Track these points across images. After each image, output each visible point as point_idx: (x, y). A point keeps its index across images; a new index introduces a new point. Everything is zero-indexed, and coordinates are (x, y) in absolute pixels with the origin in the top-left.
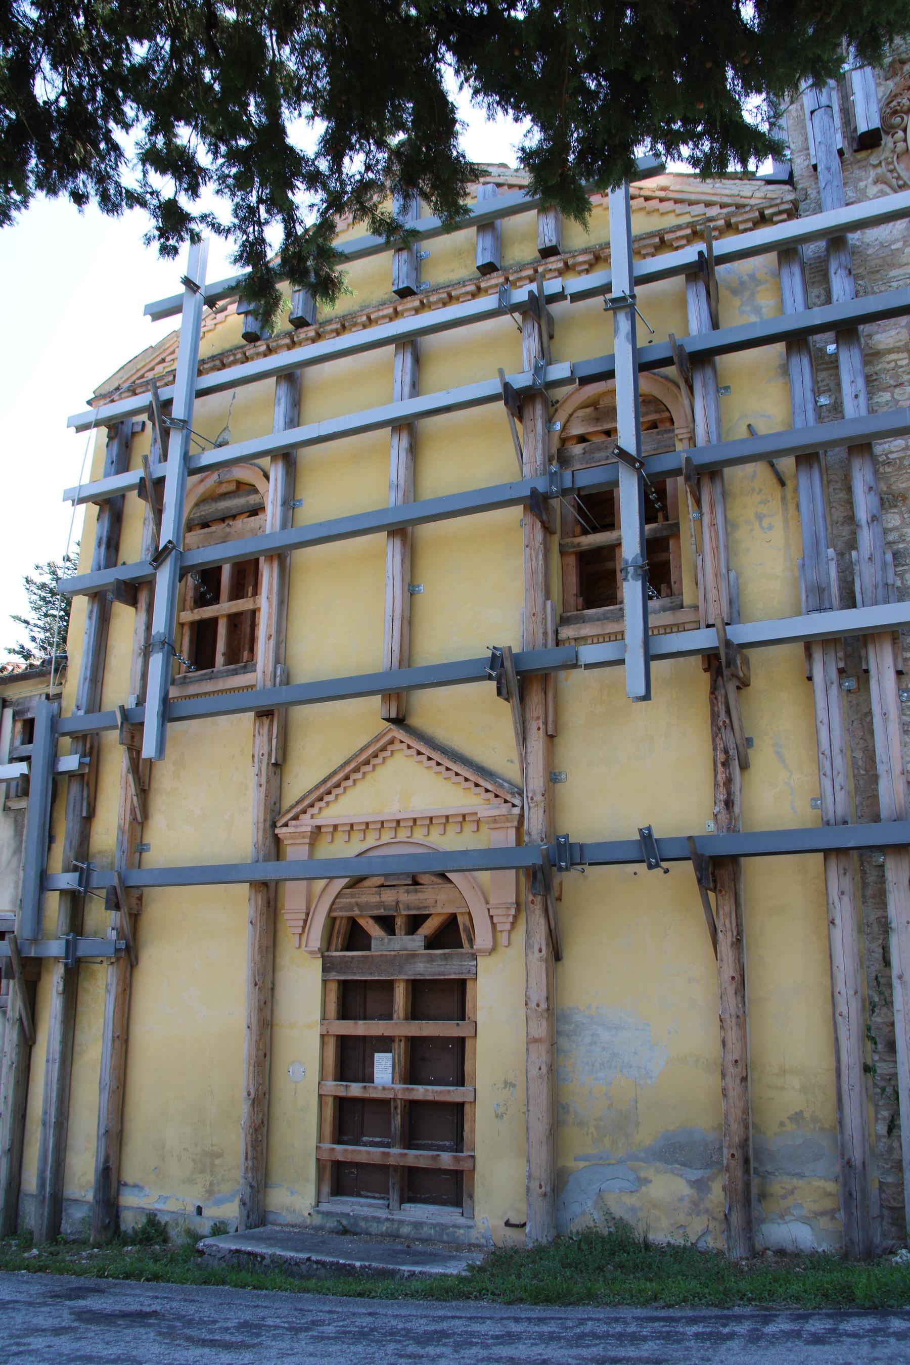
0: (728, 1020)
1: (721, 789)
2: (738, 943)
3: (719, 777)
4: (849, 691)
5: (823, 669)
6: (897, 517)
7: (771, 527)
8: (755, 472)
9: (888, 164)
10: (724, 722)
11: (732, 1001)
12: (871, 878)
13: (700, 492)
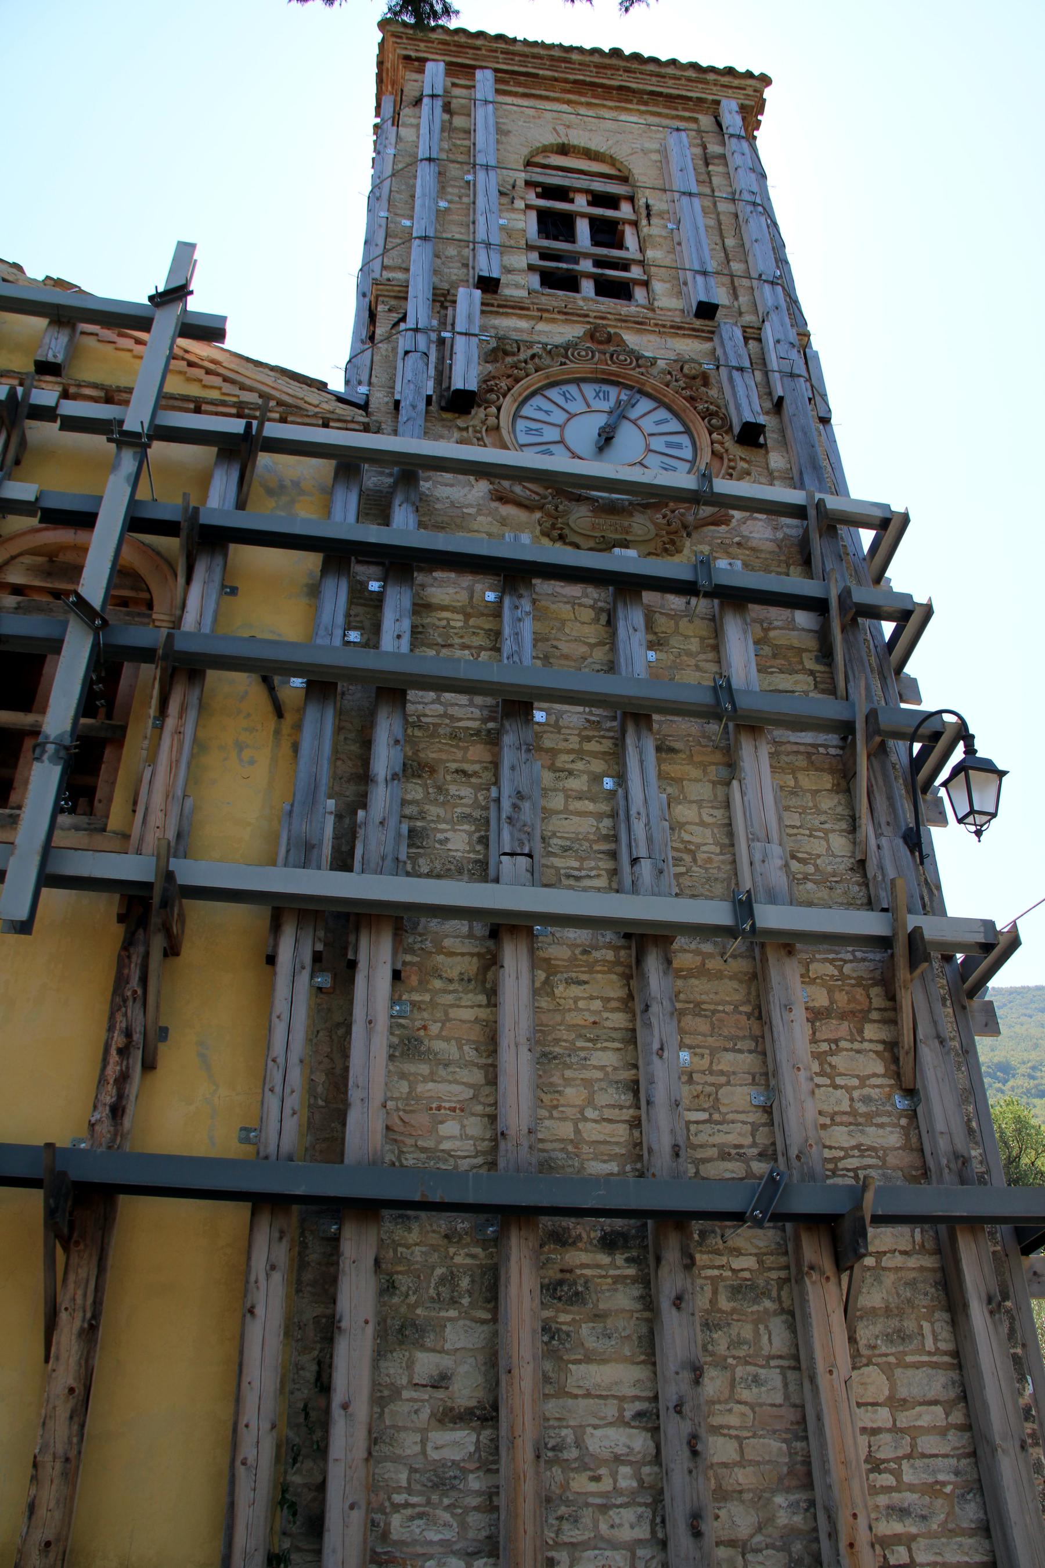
0: (49, 1465)
1: (110, 1087)
2: (90, 1332)
3: (110, 1070)
4: (320, 989)
5: (293, 949)
6: (420, 790)
7: (252, 762)
8: (246, 692)
9: (476, 431)
10: (135, 992)
11: (61, 1430)
12: (314, 1256)
13: (170, 689)
